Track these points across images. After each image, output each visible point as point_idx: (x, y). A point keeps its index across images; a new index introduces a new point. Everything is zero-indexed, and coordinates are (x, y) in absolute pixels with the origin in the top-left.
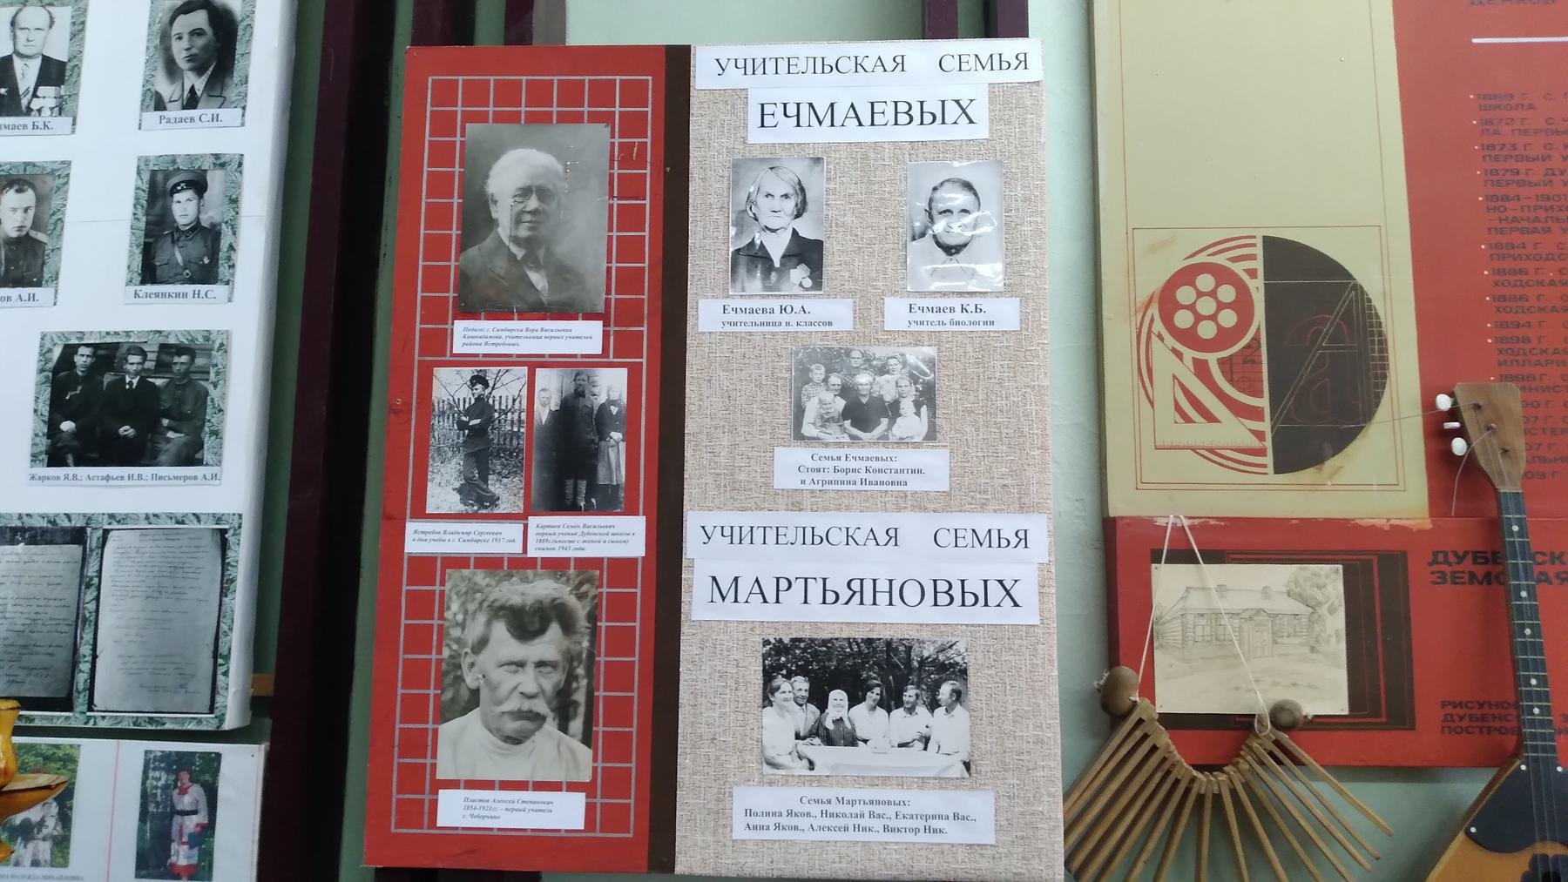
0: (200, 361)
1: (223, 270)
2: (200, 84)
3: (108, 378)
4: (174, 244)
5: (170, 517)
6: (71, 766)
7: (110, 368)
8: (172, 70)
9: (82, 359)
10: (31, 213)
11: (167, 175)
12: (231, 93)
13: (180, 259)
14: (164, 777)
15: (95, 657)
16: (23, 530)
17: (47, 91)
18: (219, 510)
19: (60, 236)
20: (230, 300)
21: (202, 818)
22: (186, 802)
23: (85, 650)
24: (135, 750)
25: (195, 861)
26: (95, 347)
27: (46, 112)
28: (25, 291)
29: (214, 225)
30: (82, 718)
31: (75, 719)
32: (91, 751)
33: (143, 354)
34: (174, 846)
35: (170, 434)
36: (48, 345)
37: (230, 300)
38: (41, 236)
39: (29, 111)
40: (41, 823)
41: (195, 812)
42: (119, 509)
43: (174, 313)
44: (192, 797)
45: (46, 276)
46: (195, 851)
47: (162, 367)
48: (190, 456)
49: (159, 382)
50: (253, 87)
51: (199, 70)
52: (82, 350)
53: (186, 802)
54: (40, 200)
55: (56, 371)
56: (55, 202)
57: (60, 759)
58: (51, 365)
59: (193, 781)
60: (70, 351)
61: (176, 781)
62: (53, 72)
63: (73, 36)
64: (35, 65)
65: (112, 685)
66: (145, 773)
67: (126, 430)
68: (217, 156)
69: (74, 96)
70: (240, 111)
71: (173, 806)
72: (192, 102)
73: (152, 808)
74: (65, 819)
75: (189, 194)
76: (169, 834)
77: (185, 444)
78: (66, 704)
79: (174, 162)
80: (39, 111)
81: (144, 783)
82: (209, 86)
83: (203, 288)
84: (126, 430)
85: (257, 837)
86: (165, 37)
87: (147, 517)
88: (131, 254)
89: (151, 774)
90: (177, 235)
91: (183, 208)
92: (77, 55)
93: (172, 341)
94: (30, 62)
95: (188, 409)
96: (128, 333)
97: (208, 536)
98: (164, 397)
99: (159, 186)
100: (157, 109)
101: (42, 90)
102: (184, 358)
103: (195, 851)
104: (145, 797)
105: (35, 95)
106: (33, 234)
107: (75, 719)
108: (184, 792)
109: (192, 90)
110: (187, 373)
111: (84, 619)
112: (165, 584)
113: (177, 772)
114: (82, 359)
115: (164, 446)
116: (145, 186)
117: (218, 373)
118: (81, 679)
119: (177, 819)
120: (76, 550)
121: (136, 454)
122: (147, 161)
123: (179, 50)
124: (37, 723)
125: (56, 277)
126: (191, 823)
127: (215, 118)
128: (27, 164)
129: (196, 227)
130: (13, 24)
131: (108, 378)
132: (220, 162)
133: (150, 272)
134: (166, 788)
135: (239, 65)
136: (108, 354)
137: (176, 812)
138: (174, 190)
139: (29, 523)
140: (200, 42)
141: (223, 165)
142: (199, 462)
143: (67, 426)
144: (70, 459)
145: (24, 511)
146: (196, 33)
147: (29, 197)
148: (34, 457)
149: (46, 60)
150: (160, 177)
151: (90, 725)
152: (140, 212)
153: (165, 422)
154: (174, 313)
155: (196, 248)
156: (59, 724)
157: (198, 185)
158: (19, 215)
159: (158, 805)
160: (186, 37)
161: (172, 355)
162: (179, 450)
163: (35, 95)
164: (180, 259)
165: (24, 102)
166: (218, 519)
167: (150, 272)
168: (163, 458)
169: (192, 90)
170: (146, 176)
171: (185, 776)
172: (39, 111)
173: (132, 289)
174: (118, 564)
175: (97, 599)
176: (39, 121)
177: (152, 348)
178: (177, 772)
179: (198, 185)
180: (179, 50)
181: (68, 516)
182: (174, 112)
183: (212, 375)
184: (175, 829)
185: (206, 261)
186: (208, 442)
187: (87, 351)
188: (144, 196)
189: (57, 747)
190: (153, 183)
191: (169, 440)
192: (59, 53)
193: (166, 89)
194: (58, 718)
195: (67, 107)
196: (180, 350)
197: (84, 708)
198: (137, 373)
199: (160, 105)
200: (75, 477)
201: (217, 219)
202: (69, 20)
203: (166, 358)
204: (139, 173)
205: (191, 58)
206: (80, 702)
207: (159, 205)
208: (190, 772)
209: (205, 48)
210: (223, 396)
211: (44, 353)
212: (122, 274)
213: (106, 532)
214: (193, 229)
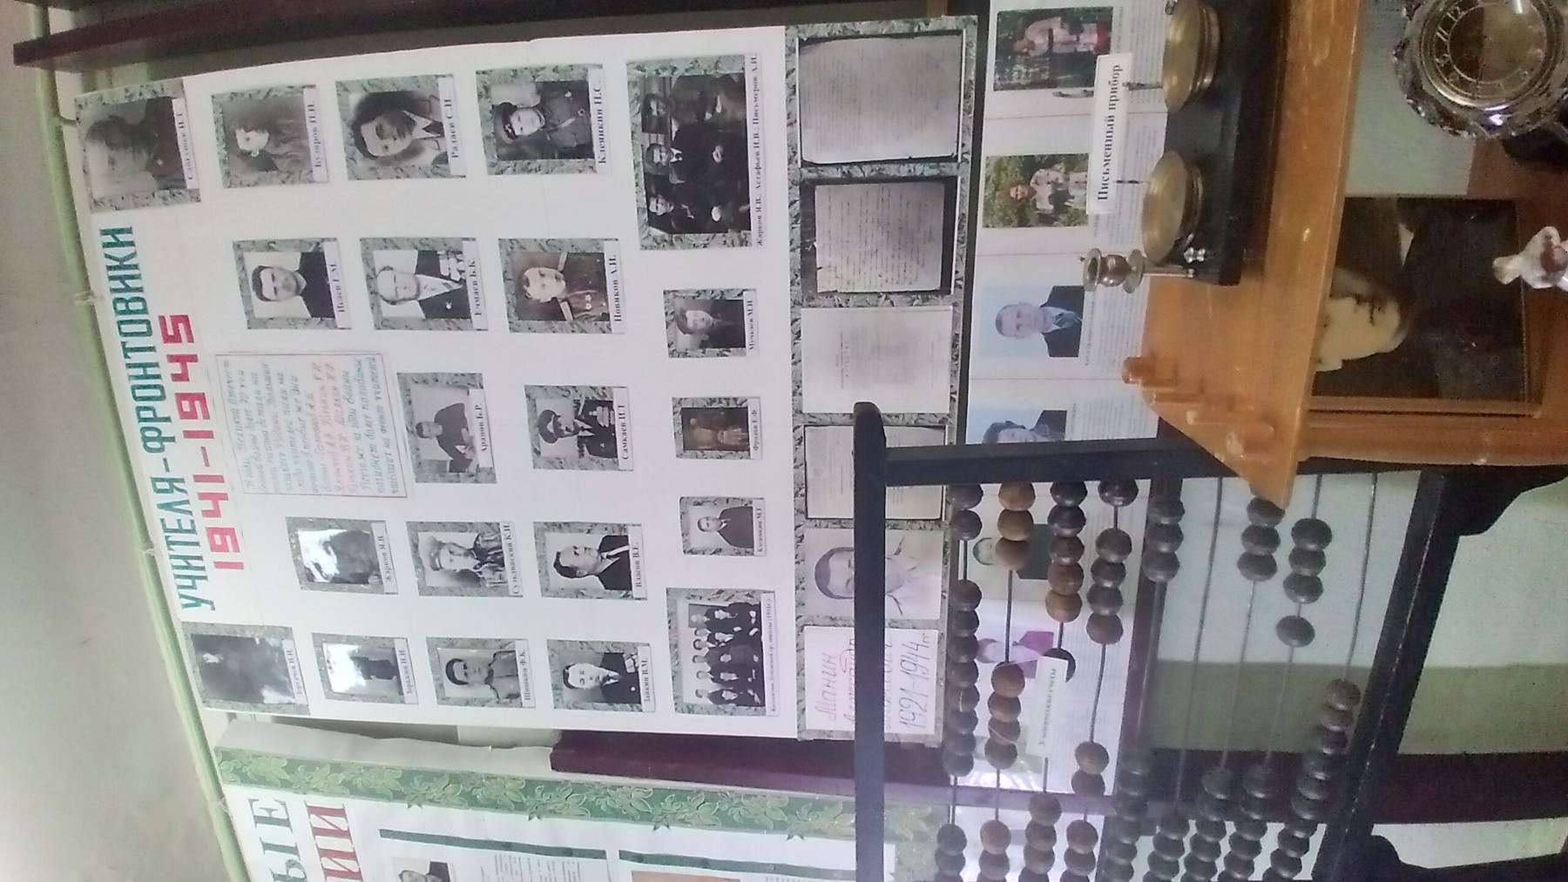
0: (655, 89)
1: (575, 76)
2: (422, 122)
3: (675, 180)
4: (551, 133)
5: (789, 101)
6: (1005, 163)
7: (666, 178)
8: (413, 151)
9: (660, 207)
10: (544, 270)
11: (500, 144)
12: (425, 91)
13: (570, 121)
14: (1019, 67)
15: (911, 160)
16: (803, 245)
17: (446, 265)
18: (783, 51)
19: (561, 241)
20: (601, 67)
21: (1056, 26)
22: (1041, 41)
23: (904, 171)
24: (995, 101)
25: (1093, 26)
26: (648, 196)
27: (461, 266)
28: (608, 268)
29: (539, 92)
30: (963, 166)
31: (963, 174)
32: (996, 145)
33: (652, 146)
34: (1081, 49)
35: (719, 110)
36: (650, 242)
37: (601, 67)
38: (563, 259)
39: (462, 281)
40: (1055, 184)
41: (1051, 31)
42: (784, 155)
43: (615, 120)
44: (1036, 36)
45: (594, 250)
46: (1086, 26)
47: (662, 127)
48: (735, 87)
49: (675, 128)
50: (419, 72)
51: (410, 124)
52: (653, 209)
53: (1041, 41)
54: (533, 264)
55: (671, 232)
56: (533, 248)
57: (999, 175)
58: (667, 237)
59: (1022, 36)
60: (654, 220)
61: (1022, 54)
62: (428, 262)
63: (397, 247)
64: (425, 280)
65: (934, 139)
66: (1013, 87)
67: (717, 156)
68: (480, 96)
69: (444, 241)
70: (440, 80)
71: (1044, 55)
72: (437, 128)
73: (1045, 76)
74: (1050, 161)
75: (514, 119)
76: (1070, 55)
77: (727, 94)
78: (950, 183)
79: (488, 138)
80: (461, 272)
81: (1023, 87)
82: (423, 114)
83: (592, 94)
84: (717, 156)
85: (1503, 823)
86: (386, 161)
87: (790, 124)
88: (570, 171)
89: (1015, 81)
90: (549, 127)
91: (526, 124)
92: (412, 243)
93: (639, 119)
94: (423, 284)
95: (695, 95)
96: (636, 166)
97: (808, 57)
98: (687, 121)
99: (514, 152)
100: (446, 162)
101: (444, 272)
102: (653, 105)
103: (1086, 26)
104: (1036, 84)
105: (448, 278)
106: (561, 267)
107: (963, 174)
108: (1032, 45)
109: (427, 129)
110: (665, 100)
111: (879, 176)
112: (847, 97)
113: (1014, 54)
114: (660, 207)
115: (729, 115)
116: (512, 163)
117: (664, 69)
118: (928, 171)
119: (1057, 49)
120: (820, 191)
121: (736, 140)
122: (493, 165)
123: (397, 147)
124: (966, 211)
125: (595, 242)
126: (1060, 34)
127: (448, 103)
128: (505, 279)
129: (541, 108)
130: (394, 303)
131: (675, 180)
132: (485, 92)
133: (583, 151)
134: (1028, 64)
135: (402, 87)
136: (655, 183)
137: (1050, 52)
138: (512, 135)
139: (798, 242)
140: (387, 127)
141: (487, 89)
142: (742, 77)
143: (716, 214)
144: (743, 208)
145: (788, 247)
146: (380, 133)
147: (531, 274)
148: (744, 243)
149: (420, 270)
150: (503, 151)
151: (969, 157)
152: (534, 166)
153: (708, 116)
154: (615, 120)
155: (559, 107)
156: (967, 189)
157: (505, 112)
158: (546, 281)
159: (1042, 71)
160: (385, 142)
161: (651, 117)
162: (730, 98)
163: (448, 278)
164: (570, 121)
165: (456, 286)
166: (791, 51)
167: (583, 151)
168: (739, 115)
169: (427, 129)
170: (504, 164)
171: (1019, 45)
172: (461, 272)
173: (598, 166)
174: (832, 148)
175: (859, 164)
176: (469, 270)
177: (646, 139)
178: (1014, 54)
179: (505, 112)
180: (397, 147)
181: (792, 204)
182: (447, 145)
183: (666, 74)
184: (1064, 50)
185: (569, 94)
186: (724, 70)
187: (653, 202)
188: (521, 163)
189: (987, 179)
190: (509, 157)
191: (724, 110)
192: (411, 258)
193: (428, 157)
194: (962, 189)
195: (454, 246)
196: (646, 110)
197: (954, 165)
198: (669, 152)
199: (443, 159)
200: (758, 201)
201: (532, 88)
202: (385, 252)
203: (654, 123)
204: (502, 172)
205: (401, 134)
206: (949, 169)
207: (524, 147)
208: (1014, 41)
209: (392, 123)
210: (685, 60)
211: (658, 244)
212: (587, 177)
213: (805, 164)
214: (543, 111)
